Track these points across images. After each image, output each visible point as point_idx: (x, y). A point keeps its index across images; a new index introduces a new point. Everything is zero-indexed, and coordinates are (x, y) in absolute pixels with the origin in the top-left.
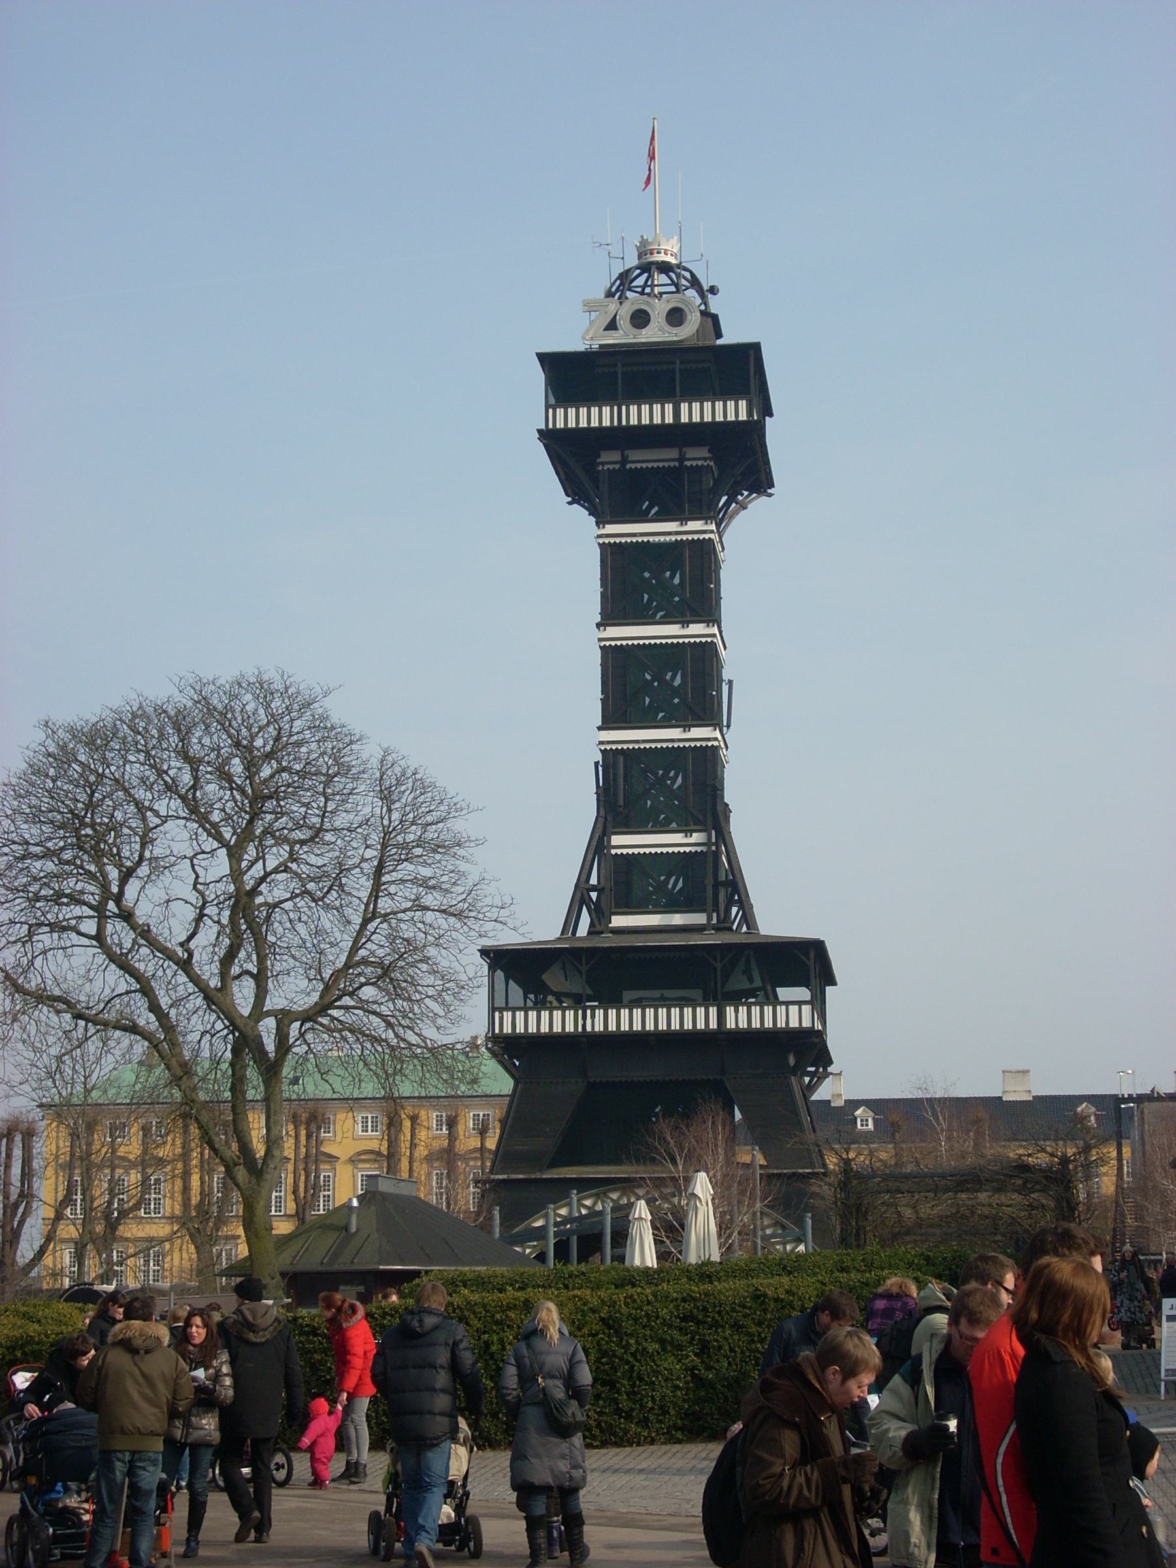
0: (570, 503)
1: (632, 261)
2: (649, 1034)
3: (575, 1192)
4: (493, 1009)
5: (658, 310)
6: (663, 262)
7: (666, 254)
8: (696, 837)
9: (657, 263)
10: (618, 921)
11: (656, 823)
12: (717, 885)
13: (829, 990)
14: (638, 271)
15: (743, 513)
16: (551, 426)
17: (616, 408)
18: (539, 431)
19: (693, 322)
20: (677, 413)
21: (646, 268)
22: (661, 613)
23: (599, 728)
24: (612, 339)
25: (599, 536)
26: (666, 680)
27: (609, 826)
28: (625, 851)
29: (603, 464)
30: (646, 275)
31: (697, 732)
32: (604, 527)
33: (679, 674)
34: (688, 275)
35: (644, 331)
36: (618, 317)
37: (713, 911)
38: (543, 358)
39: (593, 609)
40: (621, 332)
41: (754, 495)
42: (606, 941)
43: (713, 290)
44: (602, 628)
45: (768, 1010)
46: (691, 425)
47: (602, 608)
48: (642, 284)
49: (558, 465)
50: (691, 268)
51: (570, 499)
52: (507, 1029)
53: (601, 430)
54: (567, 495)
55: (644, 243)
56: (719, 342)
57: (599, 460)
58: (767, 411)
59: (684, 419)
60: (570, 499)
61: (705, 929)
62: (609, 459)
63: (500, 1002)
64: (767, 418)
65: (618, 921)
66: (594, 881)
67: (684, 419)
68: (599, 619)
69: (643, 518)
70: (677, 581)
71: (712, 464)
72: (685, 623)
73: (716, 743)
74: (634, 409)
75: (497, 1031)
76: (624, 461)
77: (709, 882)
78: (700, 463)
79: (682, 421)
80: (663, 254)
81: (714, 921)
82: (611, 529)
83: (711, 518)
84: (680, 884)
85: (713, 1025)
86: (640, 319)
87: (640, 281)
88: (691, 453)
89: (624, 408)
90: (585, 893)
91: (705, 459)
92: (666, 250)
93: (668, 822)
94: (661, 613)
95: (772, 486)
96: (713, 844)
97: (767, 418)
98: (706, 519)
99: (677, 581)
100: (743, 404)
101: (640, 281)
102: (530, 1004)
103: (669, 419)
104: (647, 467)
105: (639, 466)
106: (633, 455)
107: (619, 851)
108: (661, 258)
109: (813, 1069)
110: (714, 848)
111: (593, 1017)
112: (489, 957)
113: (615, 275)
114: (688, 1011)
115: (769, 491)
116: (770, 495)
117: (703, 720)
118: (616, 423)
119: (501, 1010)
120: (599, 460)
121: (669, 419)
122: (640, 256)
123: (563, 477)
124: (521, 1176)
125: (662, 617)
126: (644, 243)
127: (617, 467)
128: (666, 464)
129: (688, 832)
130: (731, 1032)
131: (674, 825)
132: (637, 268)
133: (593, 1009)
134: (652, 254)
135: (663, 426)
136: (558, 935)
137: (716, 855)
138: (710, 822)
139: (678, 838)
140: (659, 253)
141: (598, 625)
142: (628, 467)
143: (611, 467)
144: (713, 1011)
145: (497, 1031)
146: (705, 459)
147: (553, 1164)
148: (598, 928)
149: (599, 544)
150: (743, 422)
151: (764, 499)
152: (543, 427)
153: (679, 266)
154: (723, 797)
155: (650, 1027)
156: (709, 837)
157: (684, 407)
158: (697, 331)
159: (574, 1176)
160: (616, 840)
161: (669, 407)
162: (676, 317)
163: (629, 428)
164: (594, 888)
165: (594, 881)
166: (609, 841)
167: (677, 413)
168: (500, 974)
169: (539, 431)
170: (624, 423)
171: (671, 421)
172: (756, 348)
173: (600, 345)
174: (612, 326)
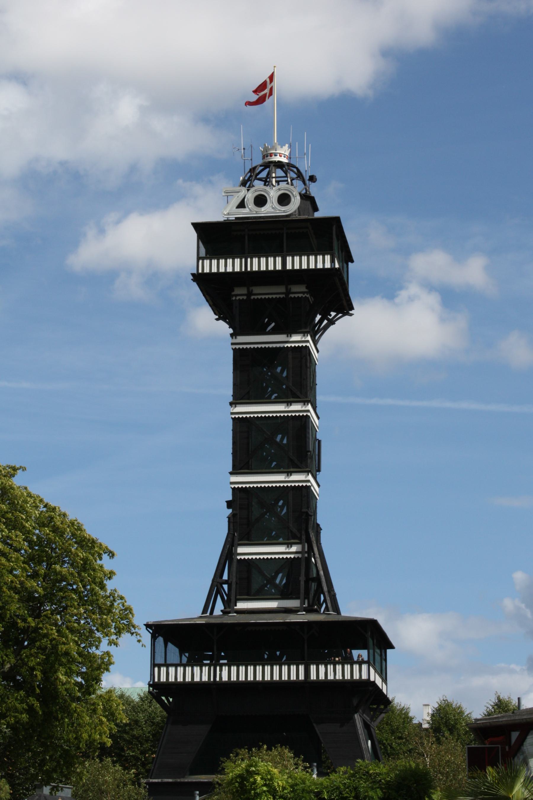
0: (217, 319)
1: (258, 161)
2: (259, 683)
3: (198, 792)
4: (154, 665)
5: (273, 194)
6: (279, 162)
7: (281, 156)
8: (294, 549)
9: (275, 162)
10: (241, 605)
11: (270, 537)
12: (308, 580)
13: (389, 651)
14: (262, 168)
15: (332, 327)
16: (200, 271)
17: (243, 260)
18: (193, 275)
19: (296, 202)
20: (284, 263)
21: (267, 165)
22: (276, 395)
23: (231, 473)
24: (244, 213)
25: (232, 344)
26: (276, 442)
27: (236, 541)
28: (246, 557)
29: (236, 295)
30: (267, 170)
31: (295, 477)
32: (236, 338)
33: (286, 438)
34: (295, 170)
35: (263, 209)
36: (246, 200)
37: (305, 598)
38: (196, 226)
39: (228, 392)
40: (247, 209)
41: (340, 315)
42: (233, 618)
43: (312, 179)
44: (234, 406)
45: (347, 667)
46: (293, 271)
47: (234, 392)
48: (265, 176)
49: (207, 296)
50: (297, 166)
51: (217, 317)
52: (163, 679)
53: (233, 273)
54: (215, 314)
55: (266, 149)
56: (317, 215)
57: (233, 293)
58: (347, 258)
59: (289, 267)
60: (217, 317)
61: (299, 611)
62: (240, 292)
63: (159, 660)
64: (350, 263)
65: (241, 605)
66: (225, 577)
67: (289, 267)
68: (231, 399)
69: (262, 332)
70: (285, 374)
71: (308, 296)
72: (289, 403)
73: (309, 484)
74: (255, 260)
75: (156, 680)
76: (250, 294)
77: (302, 579)
78: (300, 295)
79: (288, 268)
80: (278, 156)
81: (306, 605)
82: (241, 339)
83: (308, 333)
84: (284, 581)
85: (302, 677)
86: (260, 201)
87: (264, 175)
88: (295, 288)
89: (249, 260)
90: (219, 586)
91: (303, 293)
92: (280, 153)
93: (277, 537)
94: (276, 395)
95: (352, 308)
96: (306, 552)
97: (350, 263)
98: (304, 333)
99: (285, 374)
100: (328, 258)
101: (264, 175)
102: (185, 660)
103: (279, 267)
104: (265, 298)
105: (259, 297)
106: (257, 290)
107: (243, 557)
108: (277, 159)
109: (375, 706)
110: (306, 555)
111: (221, 670)
112: (151, 629)
113: (247, 170)
114: (276, 668)
115: (350, 312)
116: (351, 315)
117: (300, 468)
118: (243, 270)
119: (159, 666)
120: (233, 293)
121: (279, 267)
122: (264, 157)
123: (211, 303)
124: (170, 780)
125: (276, 398)
126: (266, 149)
127: (245, 298)
128: (278, 296)
129: (289, 545)
130: (313, 682)
131: (281, 540)
132: (261, 166)
133: (221, 666)
134: (271, 156)
135: (275, 272)
136: (200, 614)
137: (308, 560)
138: (304, 537)
139: (282, 549)
140: (276, 155)
141: (231, 404)
142: (252, 297)
143: (241, 298)
144: (302, 668)
145: (156, 680)
146: (303, 293)
147: (193, 773)
148: (228, 610)
149: (232, 349)
150: (328, 269)
151: (347, 317)
152: (195, 272)
153: (289, 165)
154: (315, 519)
155: (259, 678)
156: (303, 548)
157: (289, 259)
158: (299, 208)
159: (206, 781)
160: (240, 550)
161: (279, 260)
162: (284, 199)
163: (252, 273)
164: (226, 582)
165: (225, 577)
166: (236, 550)
167: (284, 263)
168: (160, 640)
169: (193, 275)
170: (249, 269)
171: (280, 269)
172: (336, 221)
173: (236, 218)
174: (242, 205)
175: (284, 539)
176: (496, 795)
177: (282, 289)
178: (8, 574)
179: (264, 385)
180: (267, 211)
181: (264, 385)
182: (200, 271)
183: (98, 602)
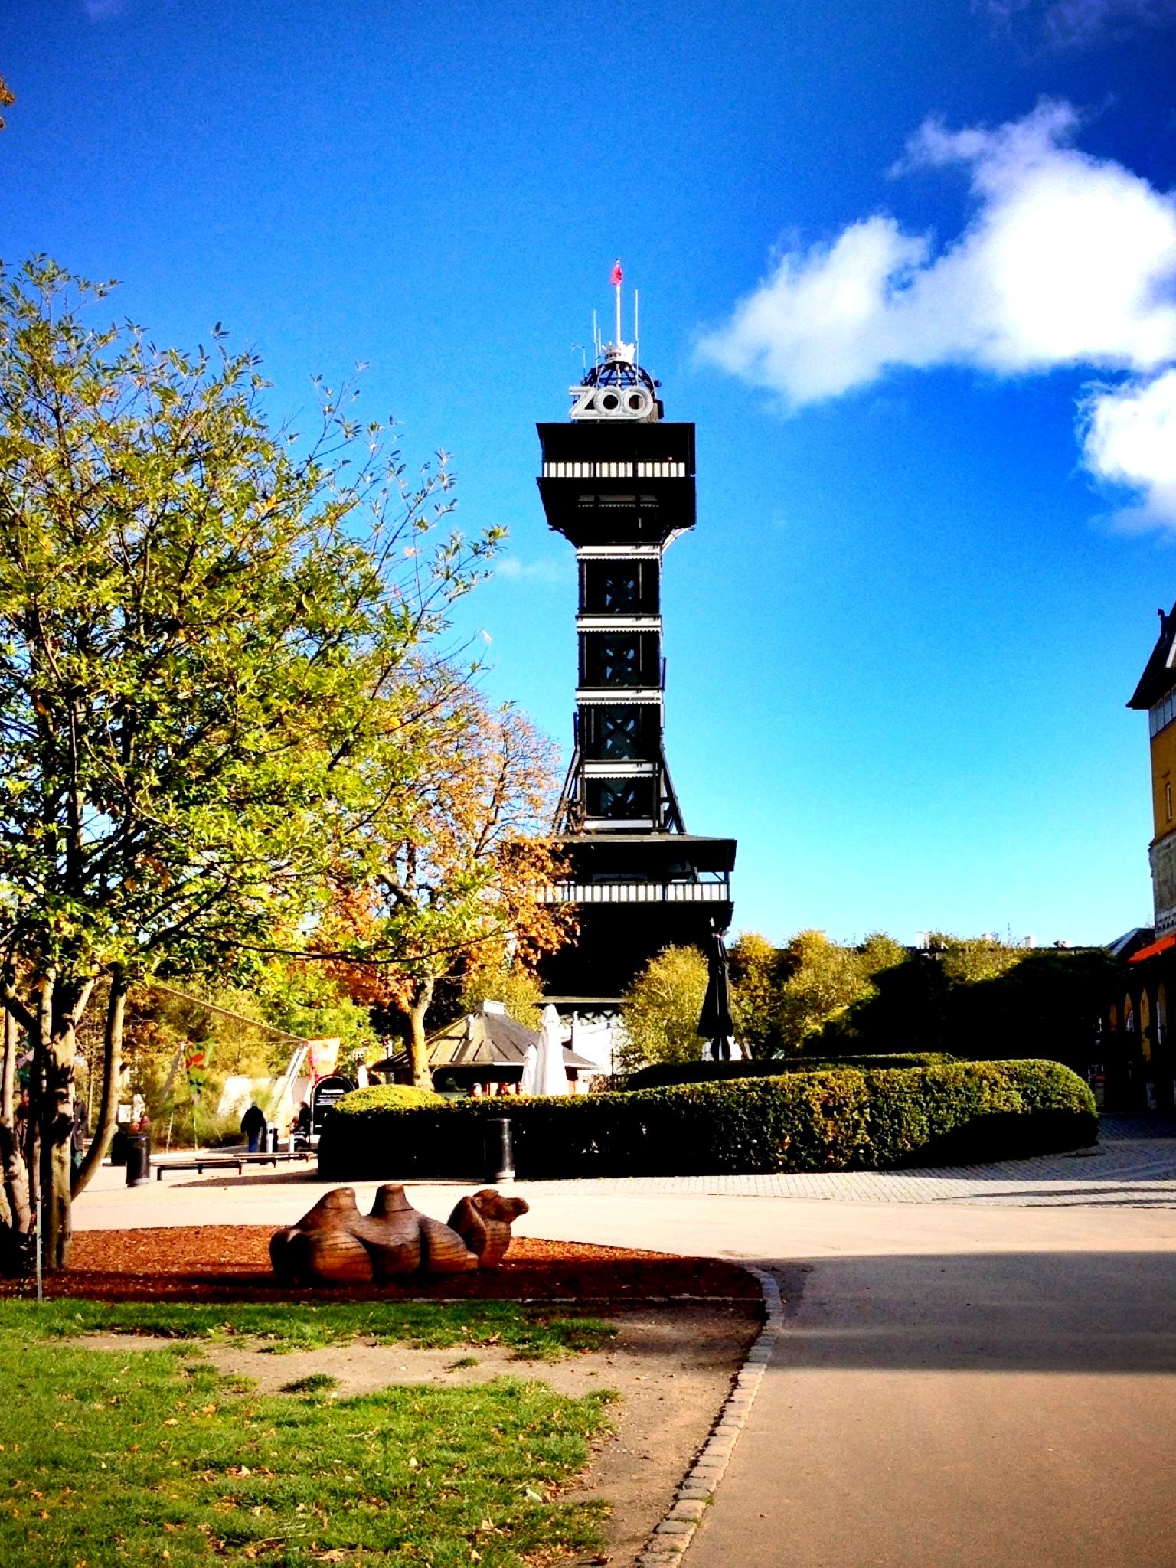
0: (551, 530)
5: (625, 394)
23: (577, 690)
24: (591, 415)
46: (645, 479)
59: (641, 474)
62: (586, 501)
67: (641, 474)
74: (605, 465)
121: (641, 466)
131: (626, 758)
141: (577, 617)
162: (634, 402)
170: (598, 475)
175: (630, 757)
176: (871, 1064)
177: (632, 498)
178: (261, 1039)
179: (608, 602)
180: (615, 414)
181: (608, 602)
182: (546, 475)
183: (464, 977)
